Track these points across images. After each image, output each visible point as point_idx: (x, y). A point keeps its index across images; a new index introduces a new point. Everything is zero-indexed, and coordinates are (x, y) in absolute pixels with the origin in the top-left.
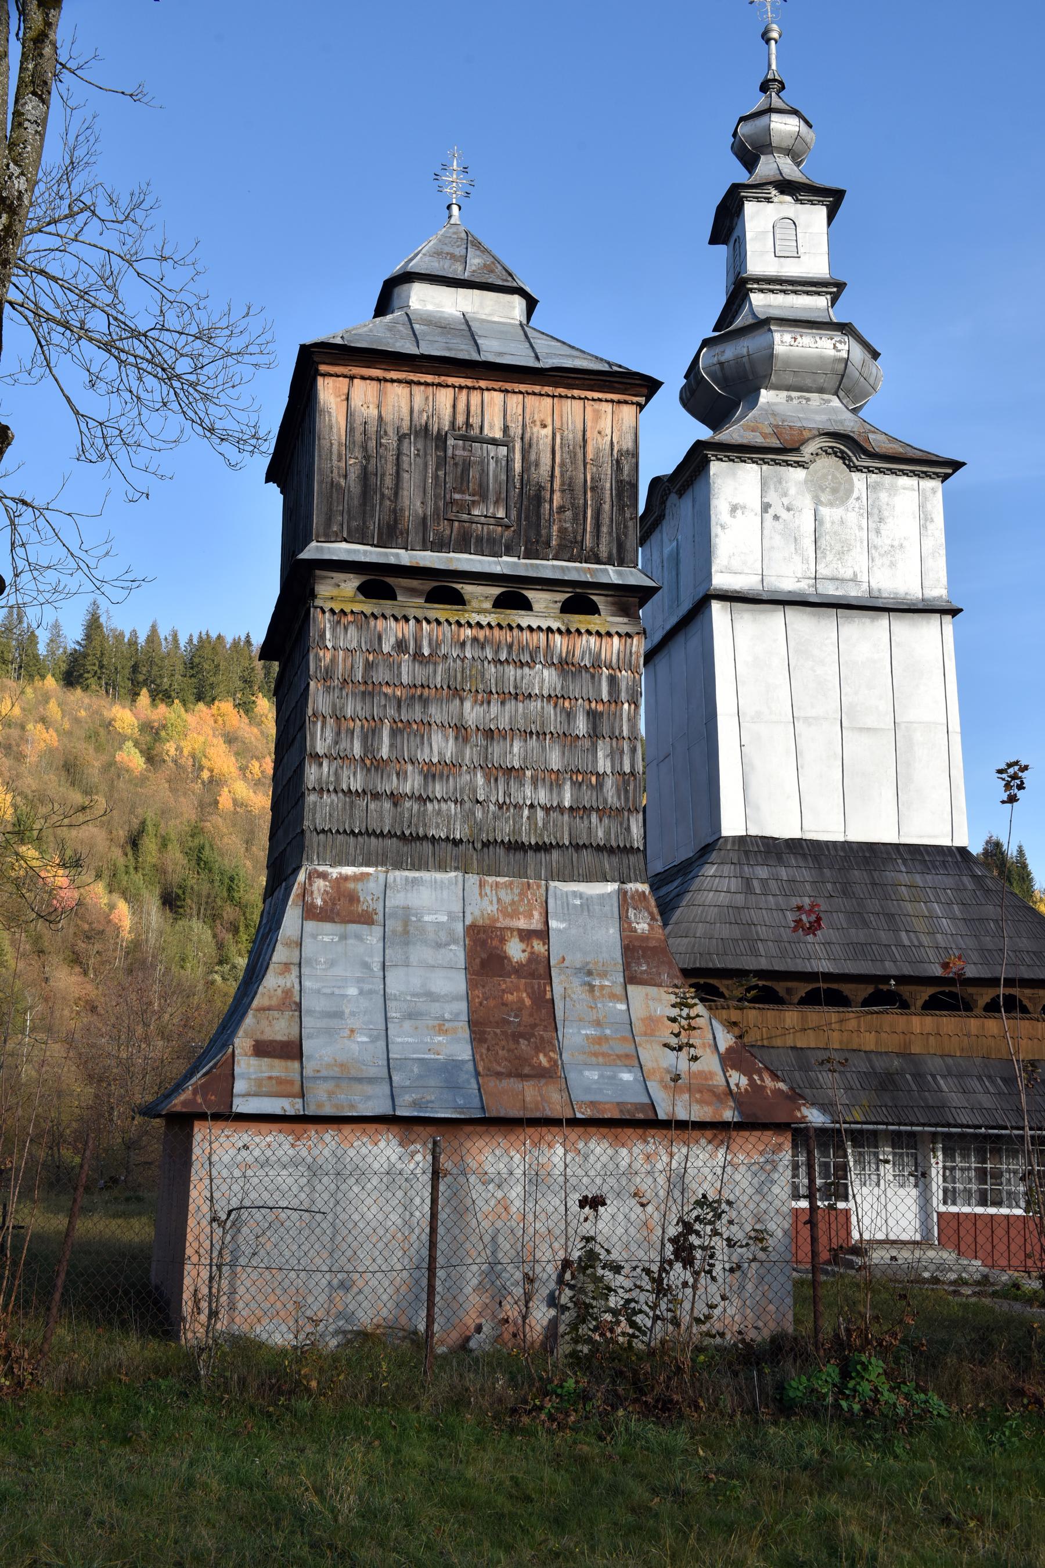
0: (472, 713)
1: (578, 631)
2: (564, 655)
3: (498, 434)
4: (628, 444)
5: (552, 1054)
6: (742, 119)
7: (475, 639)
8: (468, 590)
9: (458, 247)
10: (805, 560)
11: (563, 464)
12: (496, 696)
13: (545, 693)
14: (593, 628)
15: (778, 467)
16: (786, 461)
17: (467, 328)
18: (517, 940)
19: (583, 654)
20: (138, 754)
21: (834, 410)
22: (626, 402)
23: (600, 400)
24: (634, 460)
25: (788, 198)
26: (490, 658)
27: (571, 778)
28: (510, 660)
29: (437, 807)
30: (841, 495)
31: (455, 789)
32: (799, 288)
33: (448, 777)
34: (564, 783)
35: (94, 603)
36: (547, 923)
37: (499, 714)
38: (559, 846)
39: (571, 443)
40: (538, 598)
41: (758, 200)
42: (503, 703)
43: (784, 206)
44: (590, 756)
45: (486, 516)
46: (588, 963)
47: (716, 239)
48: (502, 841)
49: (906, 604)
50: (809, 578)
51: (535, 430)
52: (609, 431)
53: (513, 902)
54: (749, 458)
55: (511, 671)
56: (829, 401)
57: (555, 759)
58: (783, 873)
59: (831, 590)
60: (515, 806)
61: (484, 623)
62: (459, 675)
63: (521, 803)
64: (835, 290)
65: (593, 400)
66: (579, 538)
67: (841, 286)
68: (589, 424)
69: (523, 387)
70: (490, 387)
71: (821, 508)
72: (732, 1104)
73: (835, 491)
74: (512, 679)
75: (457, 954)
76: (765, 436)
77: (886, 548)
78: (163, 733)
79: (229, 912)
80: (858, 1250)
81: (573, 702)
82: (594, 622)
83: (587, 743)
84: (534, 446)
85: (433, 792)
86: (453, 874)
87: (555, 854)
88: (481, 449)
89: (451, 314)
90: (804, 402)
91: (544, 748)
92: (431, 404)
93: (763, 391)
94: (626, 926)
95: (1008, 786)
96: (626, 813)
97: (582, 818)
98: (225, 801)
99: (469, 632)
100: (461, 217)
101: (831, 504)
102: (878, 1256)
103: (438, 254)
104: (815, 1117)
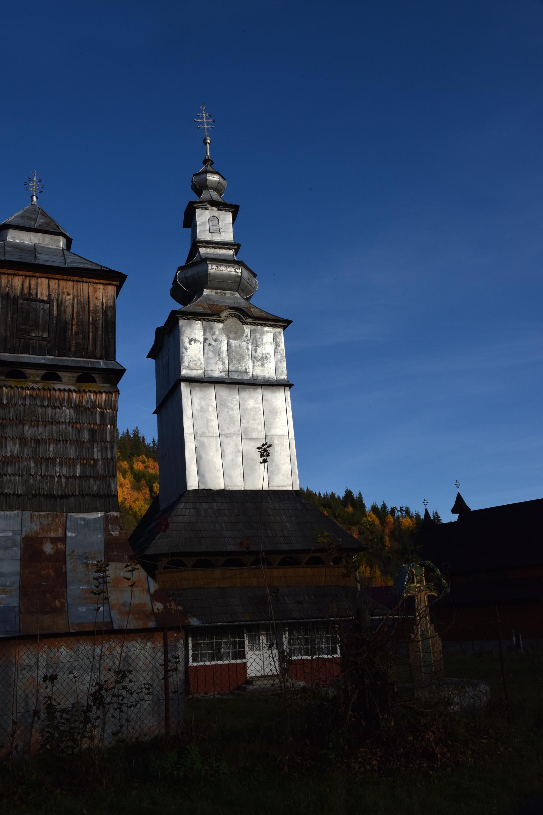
0: (28, 431)
1: (84, 391)
2: (77, 402)
3: (45, 298)
4: (111, 303)
5: (62, 600)
6: (195, 175)
7: (31, 395)
8: (28, 371)
9: (34, 214)
10: (224, 363)
11: (78, 312)
12: (42, 423)
13: (67, 421)
14: (92, 389)
15: (210, 322)
16: (213, 320)
17: (34, 250)
18: (49, 543)
19: (87, 402)
21: (237, 298)
22: (109, 284)
23: (97, 283)
24: (114, 311)
25: (215, 208)
26: (38, 404)
27: (80, 462)
28: (49, 405)
29: (9, 478)
30: (239, 335)
31: (19, 469)
32: (220, 246)
33: (15, 463)
34: (77, 464)
36: (65, 534)
37: (43, 432)
38: (73, 495)
39: (82, 302)
40: (65, 376)
41: (202, 208)
42: (45, 426)
43: (214, 212)
44: (90, 451)
45: (38, 337)
46: (86, 553)
47: (185, 226)
48: (43, 494)
49: (269, 382)
50: (225, 371)
51: (64, 296)
52: (101, 297)
53: (48, 524)
54: (197, 318)
55: (50, 410)
56: (234, 294)
57: (72, 453)
58: (215, 506)
59: (236, 377)
60: (51, 477)
61: (36, 388)
62: (22, 413)
63: (54, 474)
64: (236, 247)
65: (93, 283)
66: (86, 347)
67: (239, 246)
68: (91, 294)
69: (57, 276)
70: (41, 276)
71: (231, 341)
72: (154, 619)
73: (236, 333)
74: (50, 414)
75: (17, 552)
76: (204, 308)
77: (259, 358)
80: (250, 681)
81: (82, 425)
82: (93, 387)
83: (89, 445)
84: (64, 304)
85: (7, 471)
86: (16, 512)
87: (71, 500)
88: (36, 305)
89: (28, 244)
90: (223, 295)
91: (66, 448)
92: (10, 283)
93: (205, 290)
94: (107, 533)
95: (262, 456)
96: (108, 478)
97: (85, 481)
99: (28, 392)
100: (37, 201)
101: (235, 339)
102: (258, 684)
103: (22, 217)
104: (195, 622)
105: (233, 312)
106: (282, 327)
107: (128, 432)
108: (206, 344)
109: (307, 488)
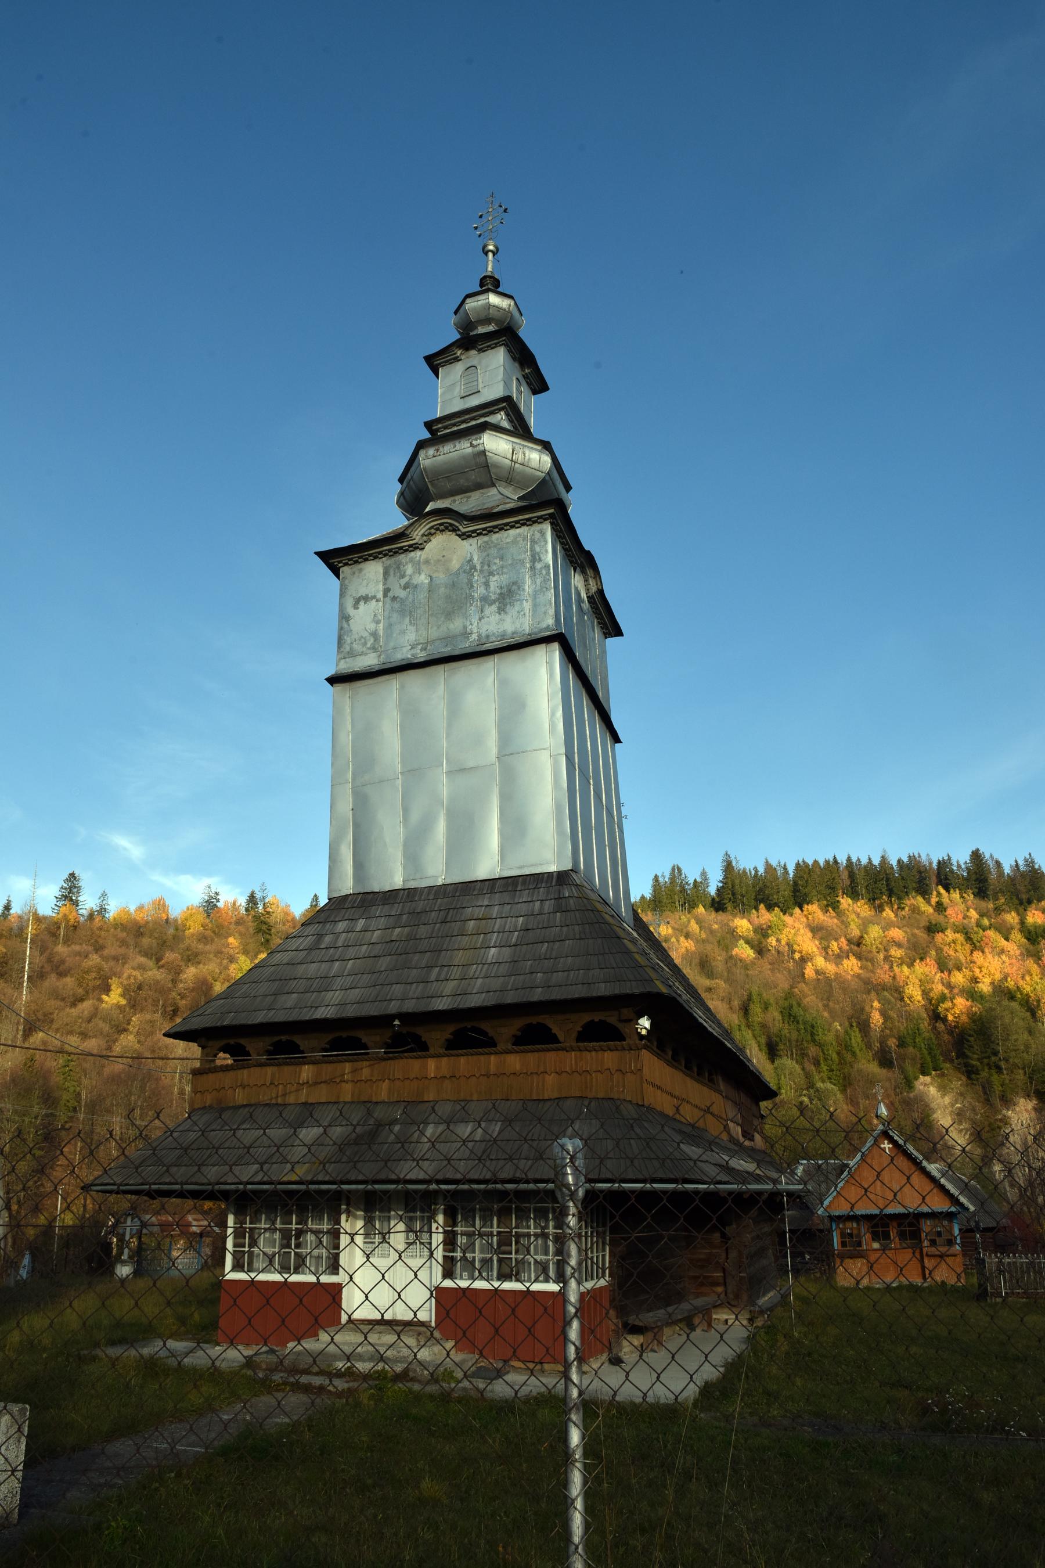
16: (401, 548)
20: (749, 948)
35: (726, 854)
78: (770, 932)
79: (813, 1051)
98: (809, 971)
105: (439, 522)
106: (545, 520)
107: (1017, 865)
108: (388, 599)
109: (767, 862)
